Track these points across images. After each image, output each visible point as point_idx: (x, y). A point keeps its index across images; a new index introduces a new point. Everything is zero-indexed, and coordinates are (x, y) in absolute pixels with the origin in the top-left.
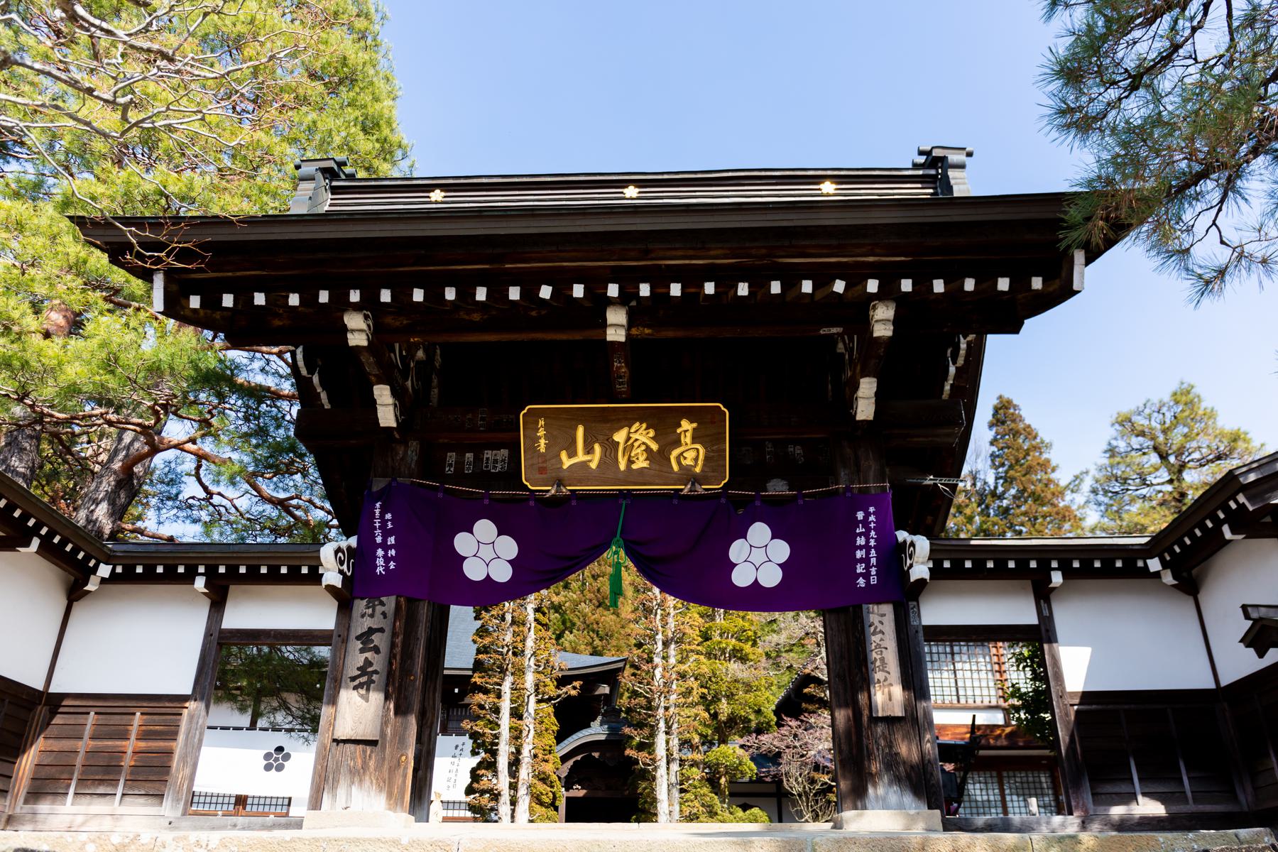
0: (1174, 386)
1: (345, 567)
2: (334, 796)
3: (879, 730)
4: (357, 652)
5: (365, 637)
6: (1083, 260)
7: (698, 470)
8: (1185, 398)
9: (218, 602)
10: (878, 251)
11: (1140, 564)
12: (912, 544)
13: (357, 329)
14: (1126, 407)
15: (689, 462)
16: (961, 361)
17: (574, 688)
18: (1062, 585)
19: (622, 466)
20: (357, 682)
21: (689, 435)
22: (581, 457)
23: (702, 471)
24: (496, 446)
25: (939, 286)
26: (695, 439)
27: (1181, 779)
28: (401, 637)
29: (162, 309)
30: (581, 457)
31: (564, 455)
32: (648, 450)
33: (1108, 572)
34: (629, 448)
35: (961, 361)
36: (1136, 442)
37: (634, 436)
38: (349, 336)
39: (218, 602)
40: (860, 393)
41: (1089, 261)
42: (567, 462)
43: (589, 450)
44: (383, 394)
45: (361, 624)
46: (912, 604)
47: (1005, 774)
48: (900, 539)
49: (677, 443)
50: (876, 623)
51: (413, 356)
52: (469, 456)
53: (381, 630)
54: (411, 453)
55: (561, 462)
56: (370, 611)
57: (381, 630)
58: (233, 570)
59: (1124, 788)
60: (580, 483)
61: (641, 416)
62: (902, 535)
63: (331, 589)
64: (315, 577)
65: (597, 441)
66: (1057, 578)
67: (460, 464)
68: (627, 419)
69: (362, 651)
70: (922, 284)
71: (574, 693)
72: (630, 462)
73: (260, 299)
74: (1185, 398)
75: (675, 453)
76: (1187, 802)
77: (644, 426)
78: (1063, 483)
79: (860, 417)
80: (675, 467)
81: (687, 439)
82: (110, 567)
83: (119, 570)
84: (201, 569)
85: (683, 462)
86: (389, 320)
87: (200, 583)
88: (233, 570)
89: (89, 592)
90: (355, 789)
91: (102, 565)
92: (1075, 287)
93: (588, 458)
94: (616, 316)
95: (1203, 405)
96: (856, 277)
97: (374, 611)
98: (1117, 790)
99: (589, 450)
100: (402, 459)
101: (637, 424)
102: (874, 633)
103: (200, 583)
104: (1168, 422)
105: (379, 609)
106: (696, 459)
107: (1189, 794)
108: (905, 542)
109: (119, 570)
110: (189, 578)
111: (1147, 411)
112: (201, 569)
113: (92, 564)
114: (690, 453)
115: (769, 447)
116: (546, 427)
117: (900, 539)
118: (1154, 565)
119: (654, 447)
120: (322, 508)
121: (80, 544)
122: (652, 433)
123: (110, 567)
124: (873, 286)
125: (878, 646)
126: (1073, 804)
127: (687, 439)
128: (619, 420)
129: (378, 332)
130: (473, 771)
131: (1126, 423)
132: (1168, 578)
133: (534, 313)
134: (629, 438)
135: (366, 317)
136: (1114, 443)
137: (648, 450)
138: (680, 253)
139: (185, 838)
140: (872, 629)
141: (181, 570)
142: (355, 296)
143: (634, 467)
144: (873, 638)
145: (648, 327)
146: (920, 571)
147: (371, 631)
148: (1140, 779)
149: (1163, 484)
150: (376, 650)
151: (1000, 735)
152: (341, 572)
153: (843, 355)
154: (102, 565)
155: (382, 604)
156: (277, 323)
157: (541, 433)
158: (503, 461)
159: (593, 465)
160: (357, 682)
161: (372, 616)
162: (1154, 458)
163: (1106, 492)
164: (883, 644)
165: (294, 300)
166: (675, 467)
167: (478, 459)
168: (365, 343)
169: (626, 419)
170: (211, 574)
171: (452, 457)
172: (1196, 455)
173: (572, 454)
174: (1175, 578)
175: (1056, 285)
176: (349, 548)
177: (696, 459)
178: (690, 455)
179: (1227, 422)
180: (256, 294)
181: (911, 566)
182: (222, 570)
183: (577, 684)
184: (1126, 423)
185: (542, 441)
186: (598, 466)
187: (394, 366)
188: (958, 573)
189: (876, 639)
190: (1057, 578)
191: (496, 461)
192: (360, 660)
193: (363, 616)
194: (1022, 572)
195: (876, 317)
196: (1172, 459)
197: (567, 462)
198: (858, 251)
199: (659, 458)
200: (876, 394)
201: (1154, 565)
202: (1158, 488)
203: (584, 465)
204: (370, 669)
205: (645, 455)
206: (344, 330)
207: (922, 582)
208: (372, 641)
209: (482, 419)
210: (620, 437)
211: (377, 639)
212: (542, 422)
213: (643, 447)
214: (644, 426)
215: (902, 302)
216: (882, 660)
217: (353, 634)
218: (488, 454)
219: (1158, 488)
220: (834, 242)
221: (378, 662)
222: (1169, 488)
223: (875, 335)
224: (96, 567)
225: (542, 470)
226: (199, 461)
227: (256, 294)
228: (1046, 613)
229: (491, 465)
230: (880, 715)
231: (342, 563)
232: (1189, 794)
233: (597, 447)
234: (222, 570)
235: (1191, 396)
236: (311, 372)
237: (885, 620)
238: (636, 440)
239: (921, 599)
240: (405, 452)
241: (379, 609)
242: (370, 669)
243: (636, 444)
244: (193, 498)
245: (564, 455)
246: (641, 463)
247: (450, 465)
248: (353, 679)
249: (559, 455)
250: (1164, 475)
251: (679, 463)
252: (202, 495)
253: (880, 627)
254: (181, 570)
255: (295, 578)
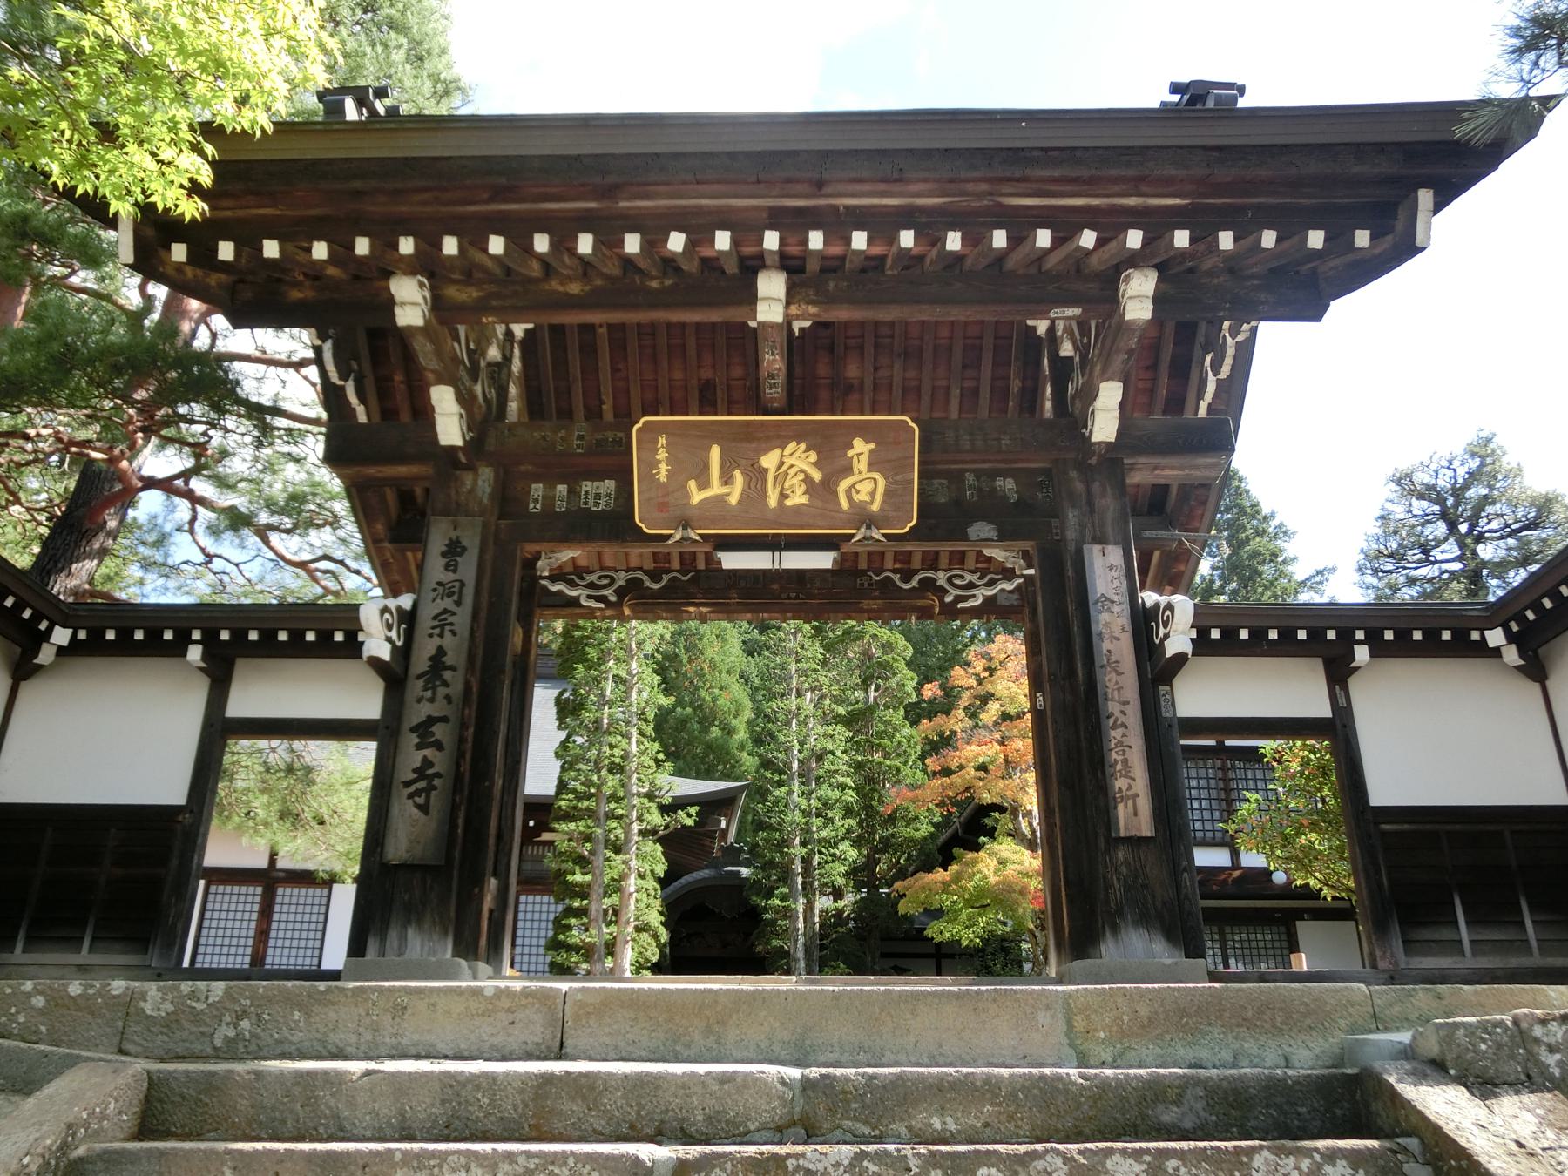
0: (1472, 437)
1: (394, 634)
2: (383, 940)
3: (1120, 855)
4: (412, 749)
5: (423, 729)
6: (1431, 206)
7: (875, 507)
8: (1483, 450)
9: (219, 676)
10: (1144, 189)
11: (1475, 636)
12: (1170, 607)
13: (410, 302)
14: (1404, 466)
15: (863, 497)
16: (1225, 371)
17: (690, 816)
18: (1368, 664)
19: (773, 502)
20: (412, 789)
21: (864, 459)
22: (717, 488)
23: (881, 509)
24: (599, 476)
25: (1226, 240)
26: (872, 466)
27: (1522, 924)
28: (471, 730)
29: (131, 260)
30: (716, 489)
31: (692, 484)
32: (808, 480)
33: (1432, 648)
34: (781, 477)
35: (1225, 371)
36: (1419, 506)
37: (788, 461)
38: (398, 311)
39: (219, 676)
40: (1099, 403)
41: (1438, 207)
42: (697, 497)
43: (727, 480)
44: (444, 399)
45: (419, 712)
46: (1163, 689)
47: (1228, 929)
48: (1149, 604)
49: (848, 470)
50: (1117, 714)
51: (484, 354)
52: (562, 489)
53: (444, 719)
54: (483, 481)
55: (688, 496)
56: (429, 694)
57: (444, 719)
58: (239, 635)
59: (1445, 934)
60: (714, 525)
61: (800, 433)
62: (1149, 598)
63: (375, 663)
64: (352, 648)
65: (738, 467)
66: (1362, 654)
67: (549, 500)
68: (779, 437)
69: (419, 747)
70: (1206, 237)
71: (690, 822)
72: (783, 496)
73: (271, 249)
74: (1483, 450)
75: (844, 485)
76: (1529, 952)
77: (803, 446)
78: (1300, 577)
79: (1097, 437)
80: (845, 504)
81: (861, 465)
82: (70, 631)
83: (82, 635)
84: (196, 635)
85: (856, 497)
86: (453, 293)
87: (195, 653)
88: (239, 635)
89: (40, 667)
90: (411, 933)
91: (57, 628)
92: (1419, 242)
93: (724, 490)
94: (772, 286)
95: (1505, 460)
96: (1111, 225)
97: (434, 694)
98: (1437, 936)
99: (727, 480)
100: (471, 491)
101: (794, 444)
102: (1114, 727)
103: (195, 653)
104: (1460, 481)
105: (442, 691)
106: (873, 494)
107: (1534, 943)
108: (1157, 605)
109: (82, 635)
110: (178, 648)
111: (1434, 467)
112: (196, 635)
113: (43, 626)
114: (864, 486)
115: (970, 479)
116: (668, 447)
117: (1149, 604)
118: (1495, 637)
119: (817, 476)
120: (357, 572)
121: (26, 596)
122: (813, 457)
123: (70, 631)
124: (1134, 239)
125: (1119, 744)
126: (1378, 953)
127: (861, 465)
128: (768, 438)
129: (439, 306)
130: (557, 921)
131: (1405, 484)
132: (1512, 655)
133: (655, 284)
134: (782, 464)
135: (421, 285)
136: (1390, 506)
137: (808, 480)
138: (866, 187)
139: (177, 988)
140: (1111, 721)
141: (168, 635)
142: (407, 246)
143: (789, 502)
144: (1113, 733)
145: (813, 303)
146: (1178, 641)
147: (431, 721)
148: (1467, 923)
149: (1453, 560)
150: (439, 746)
151: (1225, 880)
152: (389, 640)
153: (1071, 359)
154: (57, 628)
155: (446, 684)
156: (296, 295)
157: (662, 455)
158: (608, 495)
159: (733, 500)
160: (412, 789)
161: (432, 700)
162: (1441, 528)
163: (1375, 571)
164: (1126, 741)
165: (320, 251)
166: (845, 504)
167: (572, 492)
168: (420, 322)
169: (779, 437)
170: (210, 641)
171: (537, 490)
172: (1495, 525)
173: (703, 485)
174: (1521, 657)
175: (1387, 242)
176: (399, 609)
177: (873, 494)
178: (865, 489)
179: (1537, 481)
180: (266, 242)
181: (1166, 636)
182: (225, 636)
183: (693, 810)
184: (1405, 484)
185: (663, 467)
186: (739, 502)
187: (457, 361)
188: (1229, 646)
189: (1115, 734)
190: (1362, 654)
191: (598, 496)
192: (416, 759)
193: (419, 700)
194: (1314, 646)
195: (1130, 293)
196: (1463, 528)
197: (697, 497)
198: (1116, 188)
199: (823, 490)
200: (1122, 405)
201: (1495, 637)
202: (1445, 566)
203: (720, 500)
204: (430, 771)
205: (803, 487)
206: (390, 303)
207: (1180, 659)
208: (433, 734)
209: (580, 438)
210: (769, 461)
211: (439, 731)
212: (662, 441)
213: (801, 476)
214: (803, 446)
215: (1169, 268)
216: (1125, 762)
217: (406, 726)
218: (588, 486)
219: (1445, 566)
220: (1084, 173)
221: (441, 761)
222: (1457, 566)
223: (1127, 317)
224: (49, 631)
225: (662, 506)
226: (194, 510)
227: (266, 242)
228: (1342, 702)
229: (591, 501)
230: (1122, 834)
231: (390, 627)
232: (1534, 943)
233: (737, 474)
234: (225, 636)
235: (1492, 446)
236: (344, 376)
237: (1128, 709)
238: (790, 468)
239: (1177, 682)
240: (475, 482)
241: (442, 691)
242: (430, 771)
243: (792, 472)
244: (186, 562)
245: (692, 484)
246: (798, 498)
247: (536, 501)
248: (407, 784)
249: (684, 486)
250: (1451, 549)
251: (850, 498)
252: (201, 558)
253: (1122, 719)
254: (168, 635)
255: (325, 649)
